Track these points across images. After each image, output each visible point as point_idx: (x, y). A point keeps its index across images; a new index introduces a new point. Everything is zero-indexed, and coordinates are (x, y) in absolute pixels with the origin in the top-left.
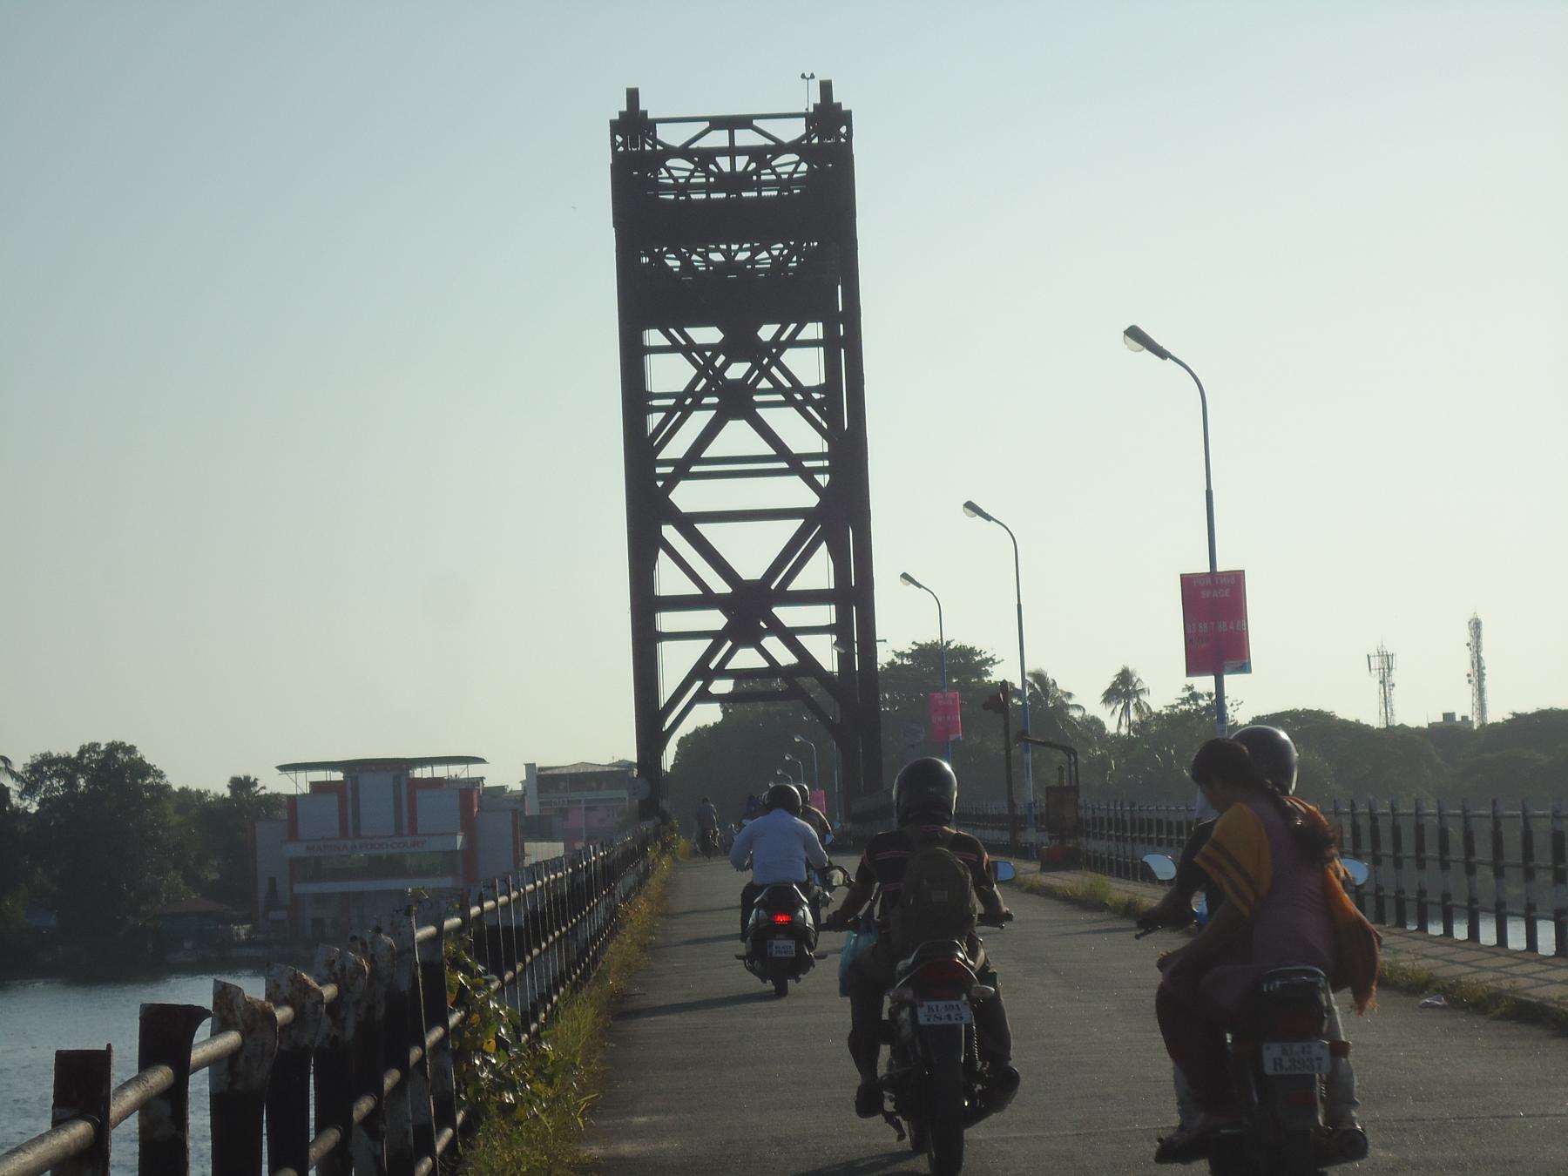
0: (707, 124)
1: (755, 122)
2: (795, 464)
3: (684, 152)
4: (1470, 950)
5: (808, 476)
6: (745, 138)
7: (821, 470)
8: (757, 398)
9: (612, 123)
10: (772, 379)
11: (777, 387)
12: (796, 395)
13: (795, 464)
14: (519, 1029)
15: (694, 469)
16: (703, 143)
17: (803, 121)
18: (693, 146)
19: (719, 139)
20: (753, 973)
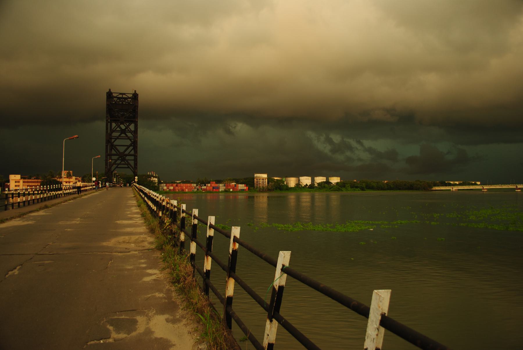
0: (119, 94)
1: (126, 94)
2: (129, 138)
3: (116, 97)
4: (324, 191)
5: (130, 140)
6: (124, 96)
7: (132, 139)
8: (126, 132)
9: (107, 93)
10: (128, 129)
11: (129, 130)
12: (130, 132)
13: (129, 138)
14: (339, 189)
15: (119, 138)
16: (118, 96)
17: (132, 95)
18: (117, 96)
19: (121, 96)
20: (405, 190)
